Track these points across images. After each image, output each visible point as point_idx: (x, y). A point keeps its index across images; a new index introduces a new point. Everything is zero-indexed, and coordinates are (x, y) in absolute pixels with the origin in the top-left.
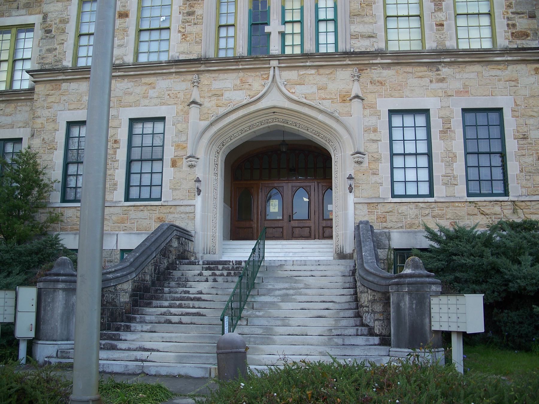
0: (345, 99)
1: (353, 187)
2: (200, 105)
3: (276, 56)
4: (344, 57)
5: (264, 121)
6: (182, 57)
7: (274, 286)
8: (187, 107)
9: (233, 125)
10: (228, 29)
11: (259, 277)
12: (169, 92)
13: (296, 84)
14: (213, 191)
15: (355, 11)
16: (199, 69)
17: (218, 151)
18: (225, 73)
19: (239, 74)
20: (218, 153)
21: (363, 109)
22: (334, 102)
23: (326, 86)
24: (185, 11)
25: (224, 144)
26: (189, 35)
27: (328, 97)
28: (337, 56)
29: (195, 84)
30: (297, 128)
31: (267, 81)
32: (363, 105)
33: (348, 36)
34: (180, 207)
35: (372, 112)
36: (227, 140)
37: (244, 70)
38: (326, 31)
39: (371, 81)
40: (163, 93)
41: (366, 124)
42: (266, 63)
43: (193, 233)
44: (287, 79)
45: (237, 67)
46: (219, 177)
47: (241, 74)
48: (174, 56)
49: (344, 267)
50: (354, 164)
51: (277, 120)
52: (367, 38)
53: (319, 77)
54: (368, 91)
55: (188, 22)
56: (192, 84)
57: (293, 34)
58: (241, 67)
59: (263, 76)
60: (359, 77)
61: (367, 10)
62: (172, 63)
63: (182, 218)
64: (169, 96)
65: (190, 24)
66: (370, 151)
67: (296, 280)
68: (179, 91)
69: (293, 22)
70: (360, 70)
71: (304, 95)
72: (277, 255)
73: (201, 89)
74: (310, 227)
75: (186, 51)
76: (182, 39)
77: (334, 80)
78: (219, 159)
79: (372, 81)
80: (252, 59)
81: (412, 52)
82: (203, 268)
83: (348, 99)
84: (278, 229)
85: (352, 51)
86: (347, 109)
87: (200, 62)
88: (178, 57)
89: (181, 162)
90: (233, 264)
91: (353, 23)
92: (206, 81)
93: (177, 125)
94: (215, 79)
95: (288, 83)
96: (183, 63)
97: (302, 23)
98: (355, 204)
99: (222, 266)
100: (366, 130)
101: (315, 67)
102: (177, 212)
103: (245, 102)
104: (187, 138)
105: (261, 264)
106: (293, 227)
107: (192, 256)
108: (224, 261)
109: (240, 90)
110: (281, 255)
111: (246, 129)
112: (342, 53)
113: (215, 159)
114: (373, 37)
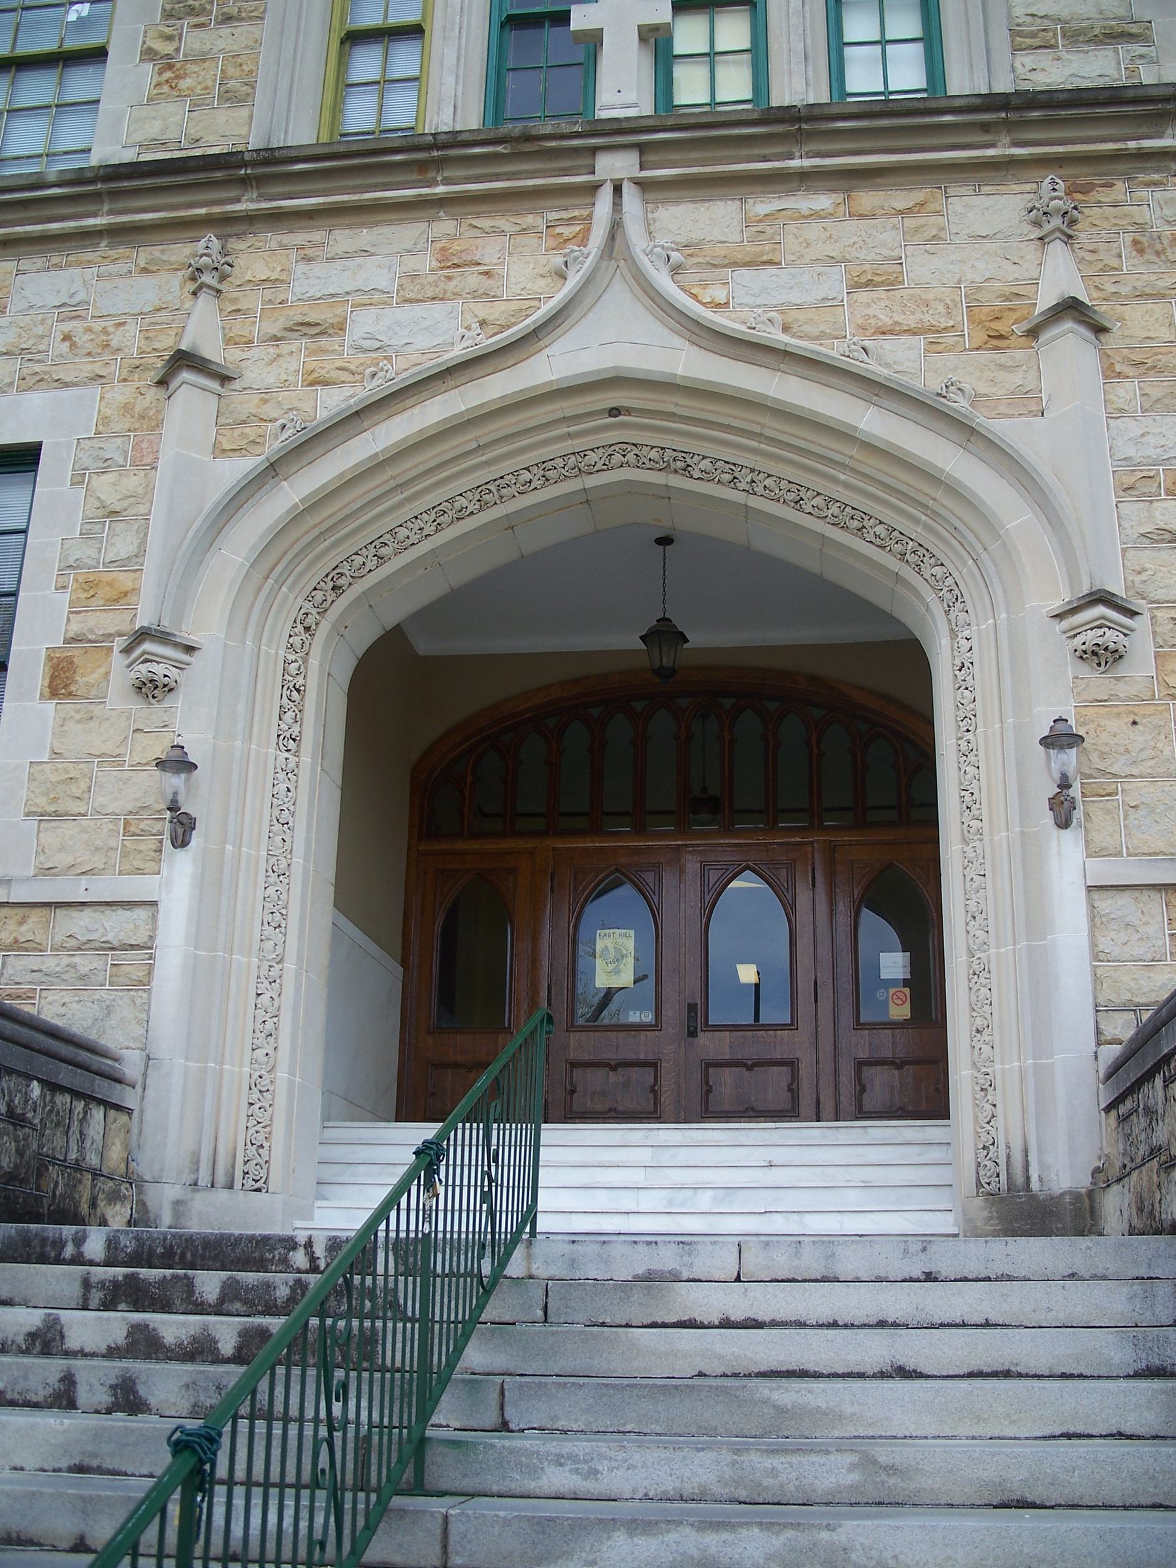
0: (999, 326)
1: (1079, 796)
2: (225, 379)
4: (985, 127)
5: (559, 462)
7: (594, 1473)
8: (153, 394)
9: (393, 478)
11: (475, 1381)
12: (68, 326)
14: (266, 828)
17: (310, 621)
20: (307, 629)
21: (1106, 377)
22: (940, 348)
25: (339, 582)
26: (191, 68)
27: (911, 321)
28: (948, 118)
29: (206, 278)
30: (739, 497)
32: (1105, 355)
33: (1001, 40)
34: (74, 913)
35: (1155, 393)
36: (359, 560)
38: (877, 38)
39: (1135, 242)
40: (39, 330)
41: (1131, 452)
42: (572, 168)
43: (131, 1068)
46: (306, 759)
47: (445, 226)
49: (1131, 1299)
50: (1071, 668)
51: (631, 457)
52: (1102, 43)
54: (1124, 290)
58: (441, 189)
60: (1073, 222)
63: (82, 978)
64: (67, 344)
66: (1161, 594)
67: (780, 1410)
68: (122, 319)
71: (780, 312)
72: (627, 1201)
73: (235, 301)
74: (791, 1064)
76: (158, 85)
78: (314, 662)
79: (1144, 240)
80: (499, 149)
82: (86, 1284)
83: (1019, 329)
84: (634, 1073)
86: (1016, 379)
89: (102, 670)
90: (313, 1259)
93: (96, 481)
96: (148, 182)
98: (1096, 895)
99: (224, 1275)
100: (1128, 481)
102: (58, 939)
103: (458, 352)
104: (143, 542)
105: (502, 1263)
106: (709, 1064)
107: (115, 1197)
108: (251, 1238)
109: (434, 299)
110: (649, 1201)
111: (463, 502)
113: (291, 657)
114: (1130, 37)
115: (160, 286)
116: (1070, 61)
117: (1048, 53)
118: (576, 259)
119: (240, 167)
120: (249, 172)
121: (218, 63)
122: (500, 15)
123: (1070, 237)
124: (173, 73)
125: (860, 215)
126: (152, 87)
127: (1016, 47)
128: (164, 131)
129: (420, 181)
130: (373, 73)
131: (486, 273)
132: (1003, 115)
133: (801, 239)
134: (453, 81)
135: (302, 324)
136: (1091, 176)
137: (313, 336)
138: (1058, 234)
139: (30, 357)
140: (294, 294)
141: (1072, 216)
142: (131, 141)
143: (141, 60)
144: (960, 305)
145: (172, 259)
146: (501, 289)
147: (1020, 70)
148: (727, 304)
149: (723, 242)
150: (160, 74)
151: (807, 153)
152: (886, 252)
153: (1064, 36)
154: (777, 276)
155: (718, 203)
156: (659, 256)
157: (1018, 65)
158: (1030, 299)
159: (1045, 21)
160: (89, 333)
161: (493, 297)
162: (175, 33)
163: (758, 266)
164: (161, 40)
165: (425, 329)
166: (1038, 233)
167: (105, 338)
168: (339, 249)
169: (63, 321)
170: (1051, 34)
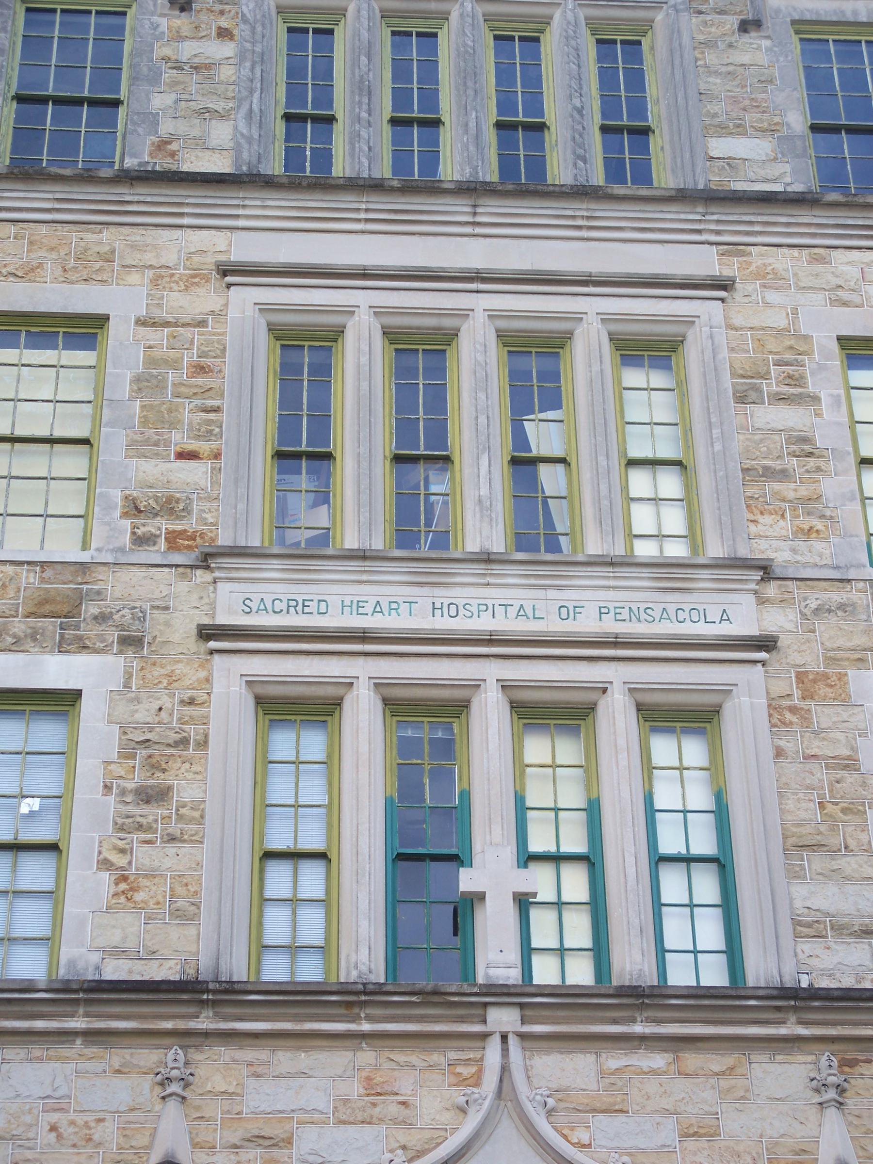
3: (512, 990)
4: (778, 1009)
6: (115, 970)
10: (300, 870)
12: (54, 1117)
13: (594, 1110)
15: (803, 830)
16: (192, 1025)
18: (299, 1048)
19: (358, 1054)
23: (714, 1122)
24: (130, 785)
26: (144, 882)
29: (174, 1088)
31: (475, 1090)
33: (786, 928)
37: (378, 1042)
40: (28, 1119)
44: (554, 1086)
45: (352, 1027)
47: (367, 1056)
48: (81, 965)
52: (859, 937)
53: (681, 1083)
55: (140, 827)
56: (158, 1090)
57: (559, 905)
59: (459, 1069)
60: (844, 1091)
61: (850, 829)
62: (76, 991)
64: (54, 1134)
65: (149, 836)
68: (101, 1115)
69: (557, 859)
70: (845, 1063)
71: (630, 1154)
73: (198, 1108)
75: (131, 944)
76: (116, 895)
77: (742, 1098)
81: (299, 988)
85: (804, 985)
87: (196, 996)
88: (98, 968)
91: (799, 877)
92: (218, 1078)
94: (259, 1070)
95: (562, 1105)
96: (124, 996)
97: (728, 868)
101: (664, 1044)
109: (363, 1122)
112: (775, 992)
115: (132, 1088)
116: (837, 951)
117: (821, 942)
118: (476, 1100)
119: (203, 992)
120: (210, 997)
121: (166, 880)
122: (392, 854)
123: (841, 1104)
124: (128, 885)
125: (687, 1075)
126: (110, 895)
127: (797, 935)
128: (125, 938)
129: (346, 1016)
130: (285, 892)
131: (404, 1103)
132: (793, 1003)
133: (643, 1092)
134: (367, 924)
135: (258, 1137)
136: (856, 1052)
137: (266, 1147)
138: (834, 1103)
139: (20, 1142)
140: (248, 1106)
141: (843, 1087)
142: (95, 945)
143: (98, 868)
144: (762, 1157)
145: (142, 1063)
146: (415, 1118)
147: (801, 956)
148: (590, 1145)
149: (584, 1090)
150: (117, 884)
151: (647, 1018)
152: (707, 1108)
153: (832, 928)
154: (627, 1123)
155: (579, 1055)
156: (539, 1102)
157: (799, 951)
158: (813, 1154)
159: (818, 913)
160: (73, 1126)
161: (410, 1125)
162: (127, 846)
163: (611, 1113)
164: (115, 852)
165: (357, 1149)
166: (817, 1099)
167: (88, 1132)
168: (283, 1069)
169: (48, 1111)
170: (822, 926)
